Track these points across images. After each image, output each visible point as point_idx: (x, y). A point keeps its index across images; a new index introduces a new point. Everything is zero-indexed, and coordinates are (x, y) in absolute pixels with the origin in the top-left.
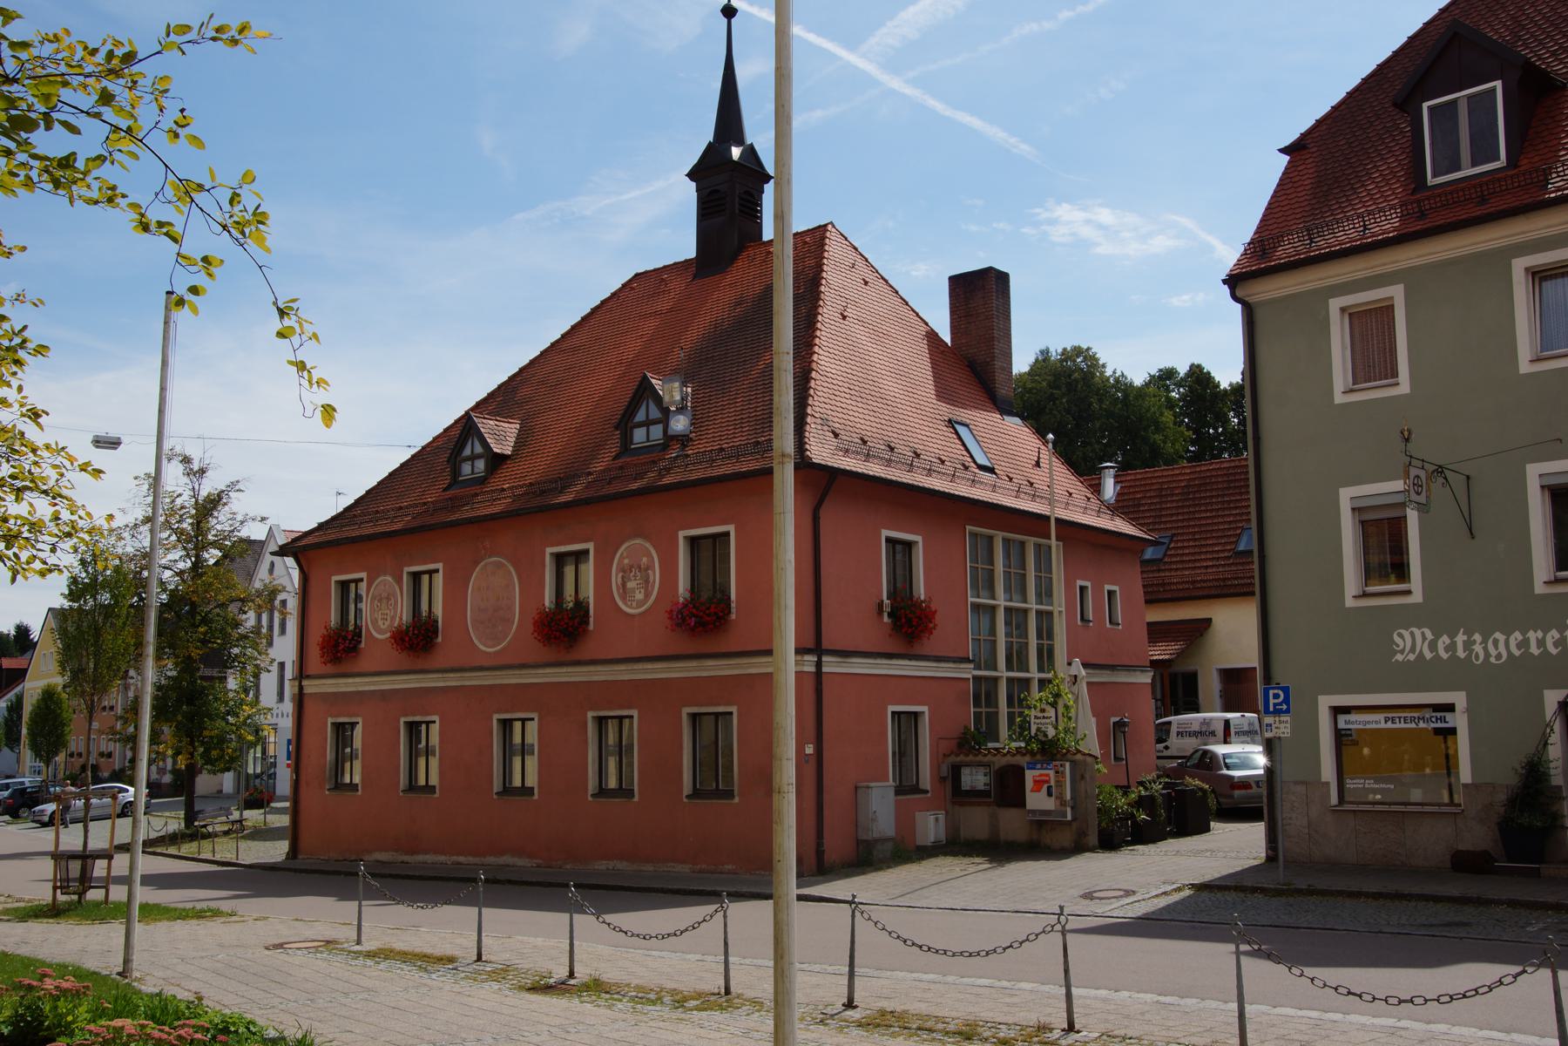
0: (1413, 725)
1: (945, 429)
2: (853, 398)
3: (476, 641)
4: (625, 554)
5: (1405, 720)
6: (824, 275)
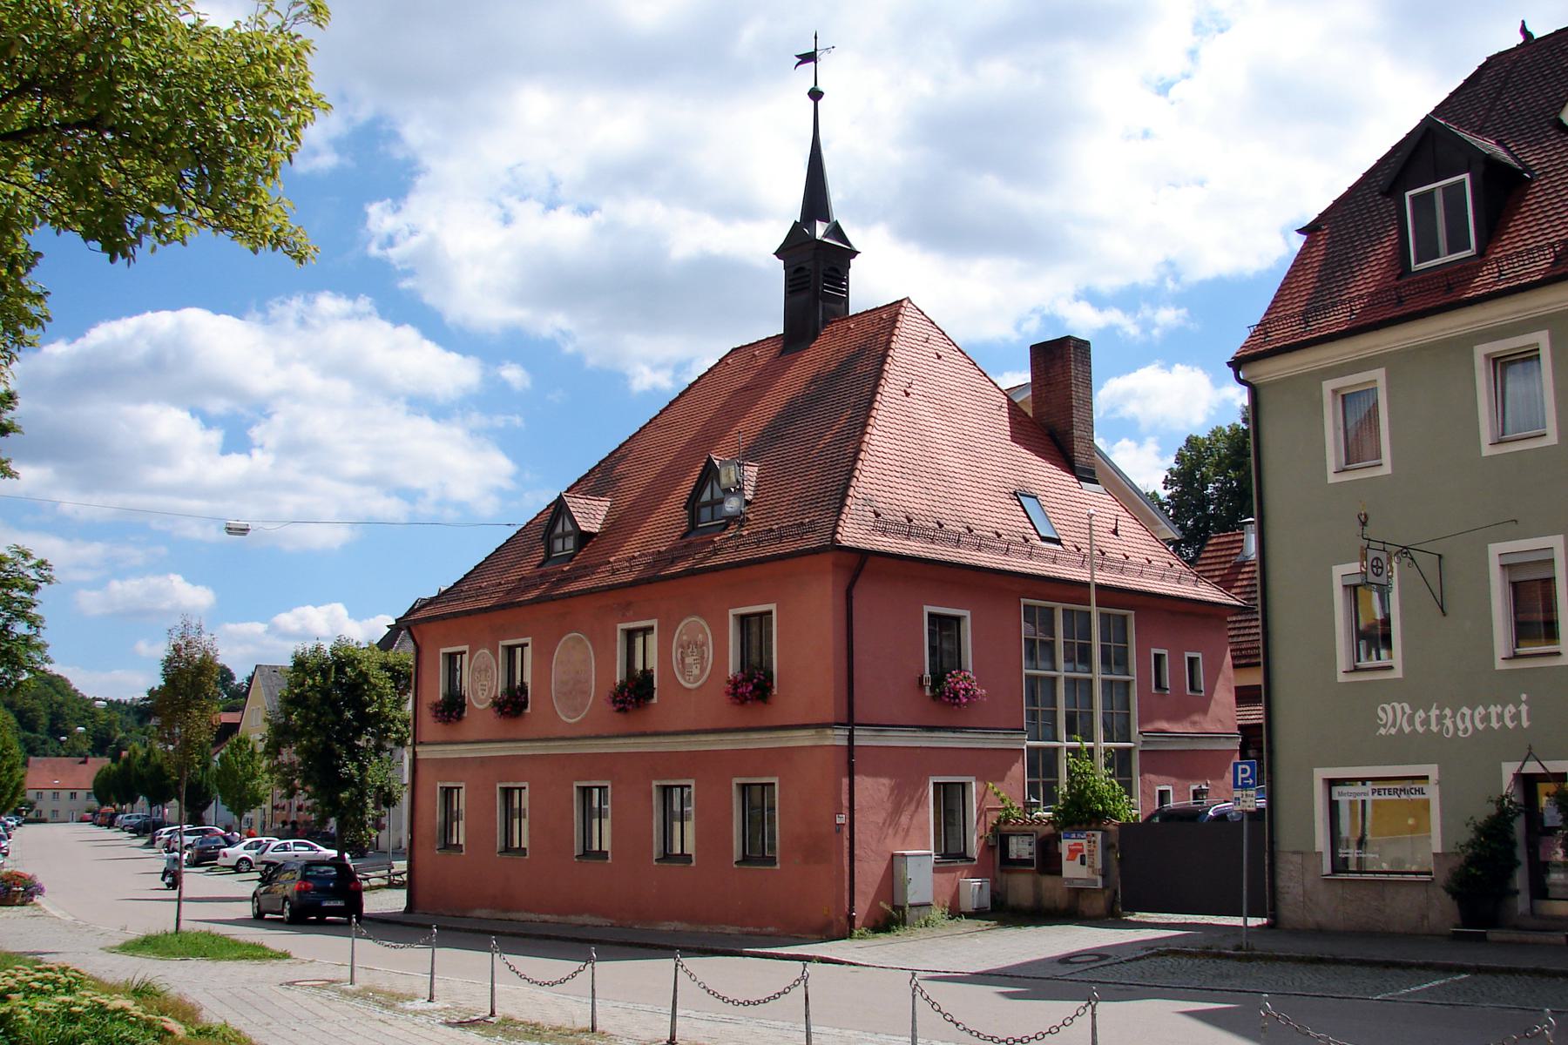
0: (1396, 797)
2: (904, 476)
3: (559, 713)
4: (684, 632)
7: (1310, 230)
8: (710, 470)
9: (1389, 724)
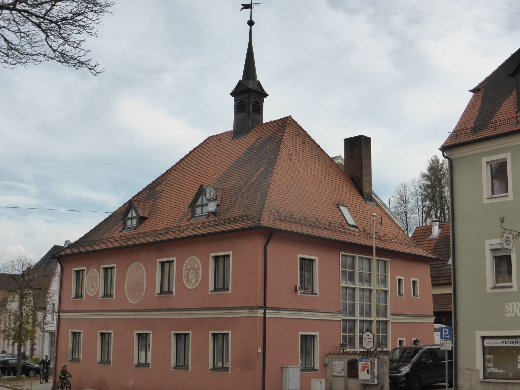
1: (335, 208)
3: (128, 299)
4: (188, 263)
5: (510, 342)
6: (283, 140)
7: (475, 91)
8: (201, 191)
9: (510, 313)
